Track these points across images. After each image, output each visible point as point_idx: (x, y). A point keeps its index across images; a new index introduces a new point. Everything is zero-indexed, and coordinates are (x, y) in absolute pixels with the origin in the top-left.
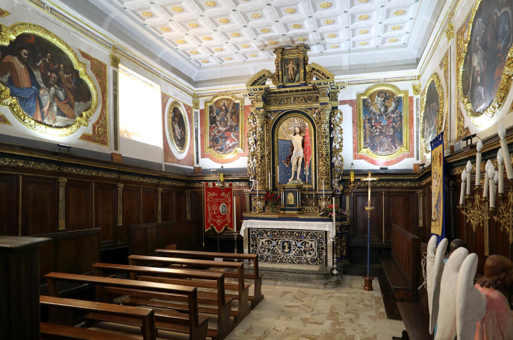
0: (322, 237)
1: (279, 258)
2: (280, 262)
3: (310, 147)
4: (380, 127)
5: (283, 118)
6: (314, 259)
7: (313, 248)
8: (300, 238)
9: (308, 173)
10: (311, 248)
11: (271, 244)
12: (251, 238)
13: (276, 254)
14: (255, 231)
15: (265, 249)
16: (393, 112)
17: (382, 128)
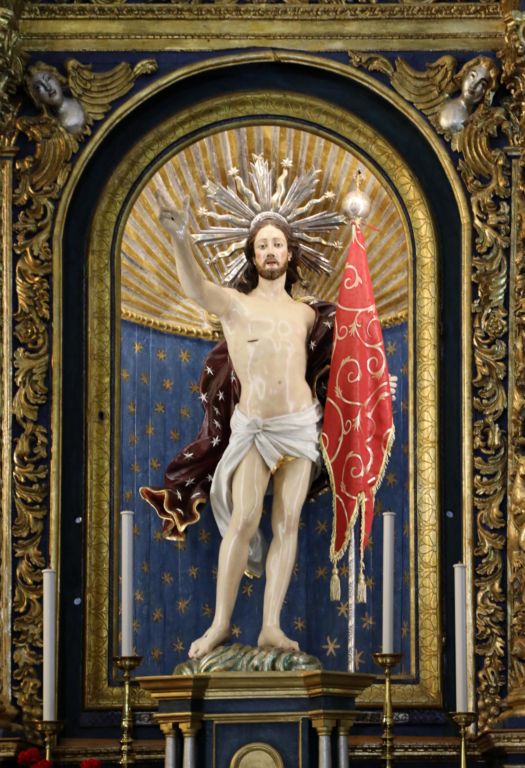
3: (377, 382)
5: (164, 128)
9: (363, 586)
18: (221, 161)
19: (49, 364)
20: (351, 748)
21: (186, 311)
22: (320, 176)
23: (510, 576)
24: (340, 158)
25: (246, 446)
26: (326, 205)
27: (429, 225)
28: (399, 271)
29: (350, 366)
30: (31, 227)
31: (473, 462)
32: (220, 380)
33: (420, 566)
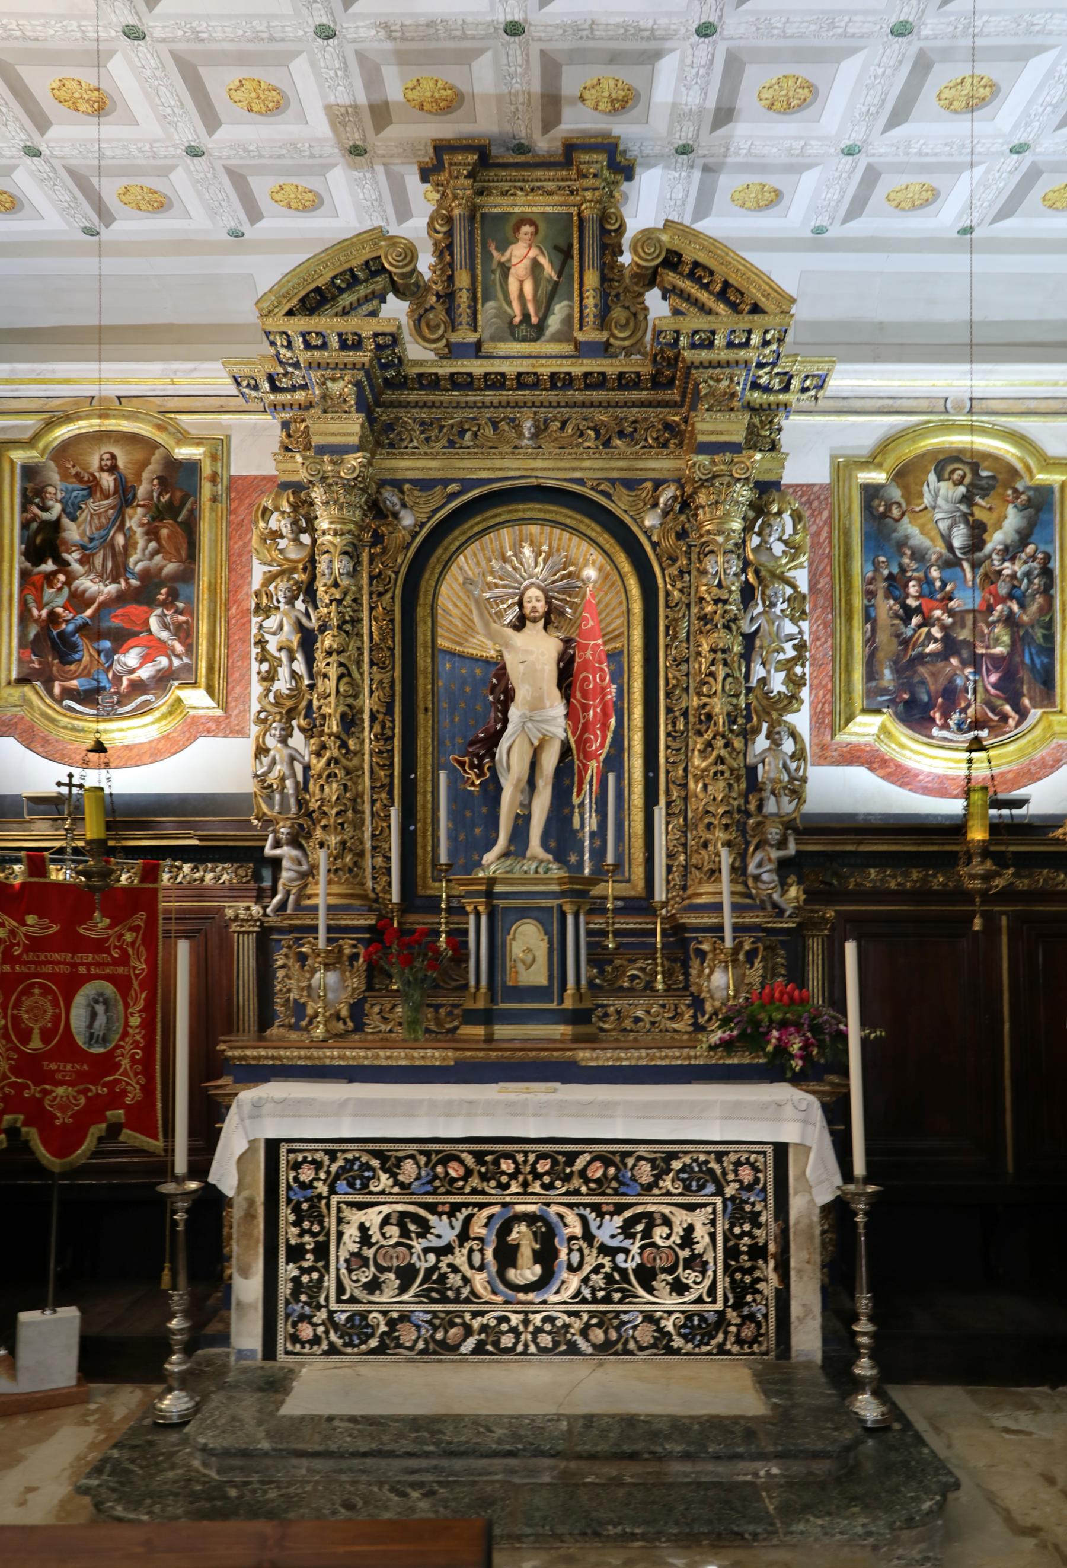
0: (757, 1180)
1: (476, 1323)
2: (479, 1349)
3: (603, 689)
4: (945, 617)
5: (466, 526)
6: (703, 1319)
7: (699, 1249)
8: (616, 1193)
9: (594, 821)
10: (686, 1253)
11: (421, 1235)
12: (289, 1201)
13: (457, 1301)
14: (318, 1156)
15: (381, 1269)
16: (1009, 553)
17: (954, 624)
18: (501, 547)
20: (588, 923)
22: (566, 557)
23: (690, 815)
24: (579, 545)
26: (570, 575)
28: (617, 617)
30: (381, 590)
32: (502, 687)
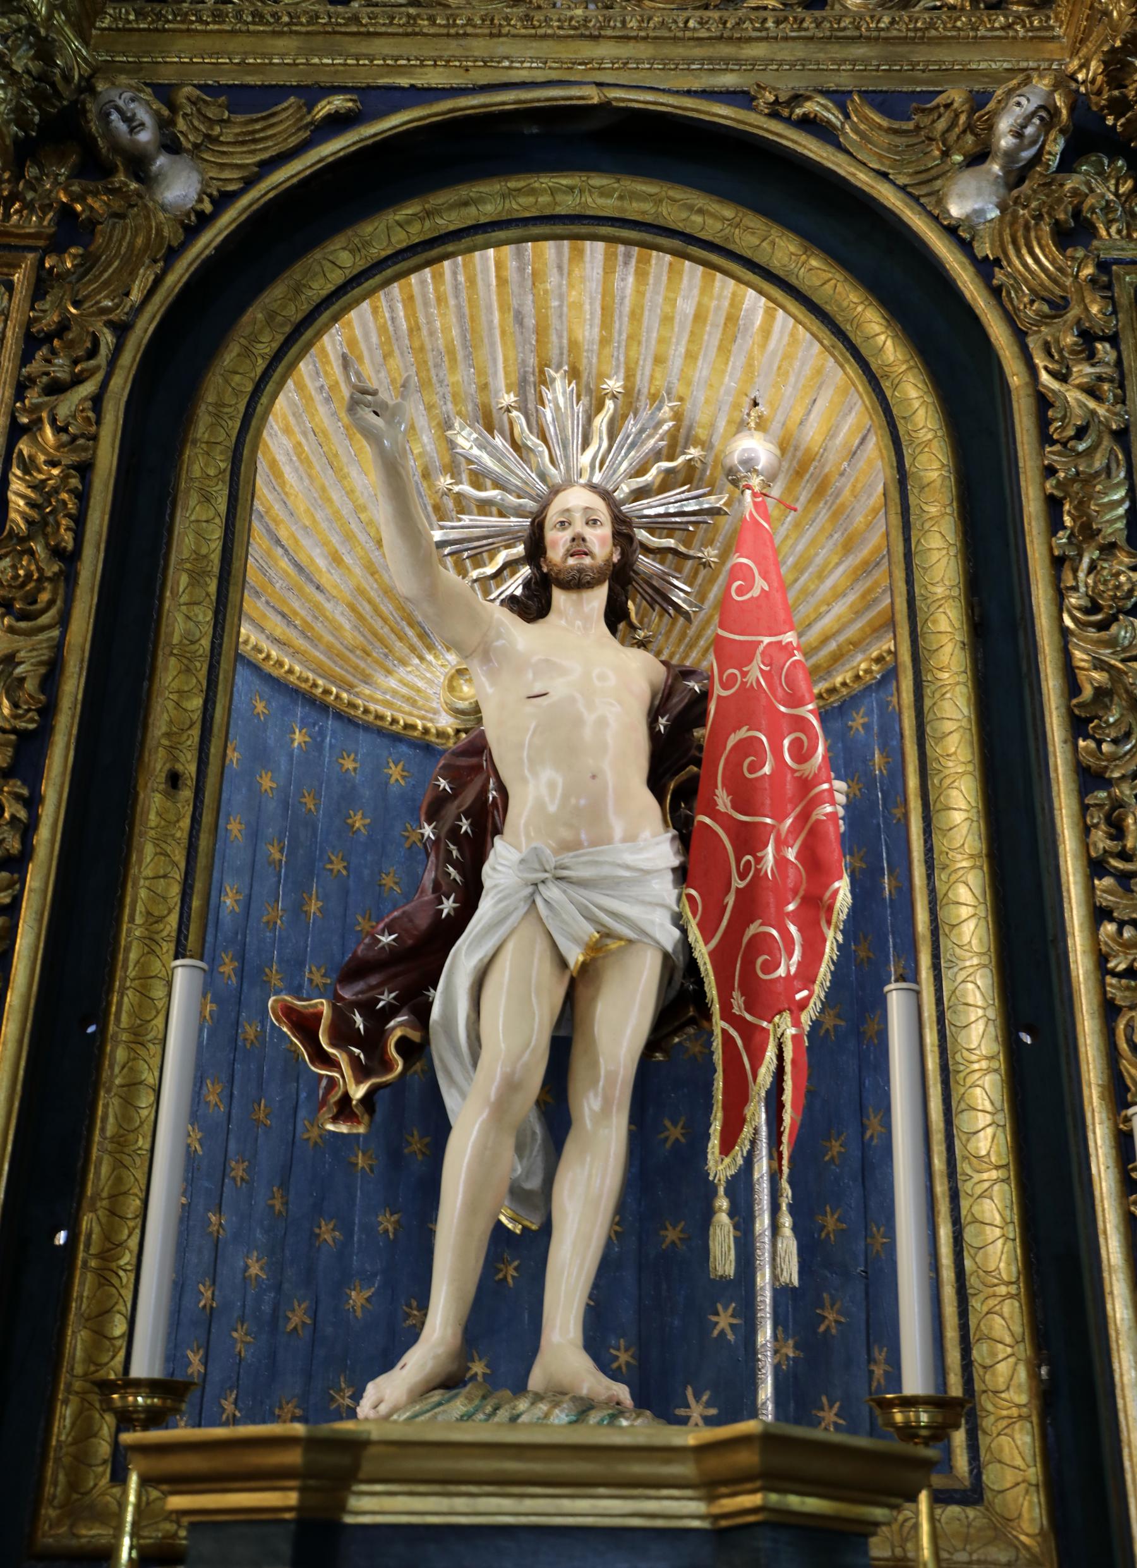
3: (805, 785)
9: (789, 1244)
19: (59, 647)
21: (404, 690)
25: (516, 909)
27: (931, 407)
28: (838, 594)
29: (748, 746)
31: (1090, 890)
33: (963, 1167)
